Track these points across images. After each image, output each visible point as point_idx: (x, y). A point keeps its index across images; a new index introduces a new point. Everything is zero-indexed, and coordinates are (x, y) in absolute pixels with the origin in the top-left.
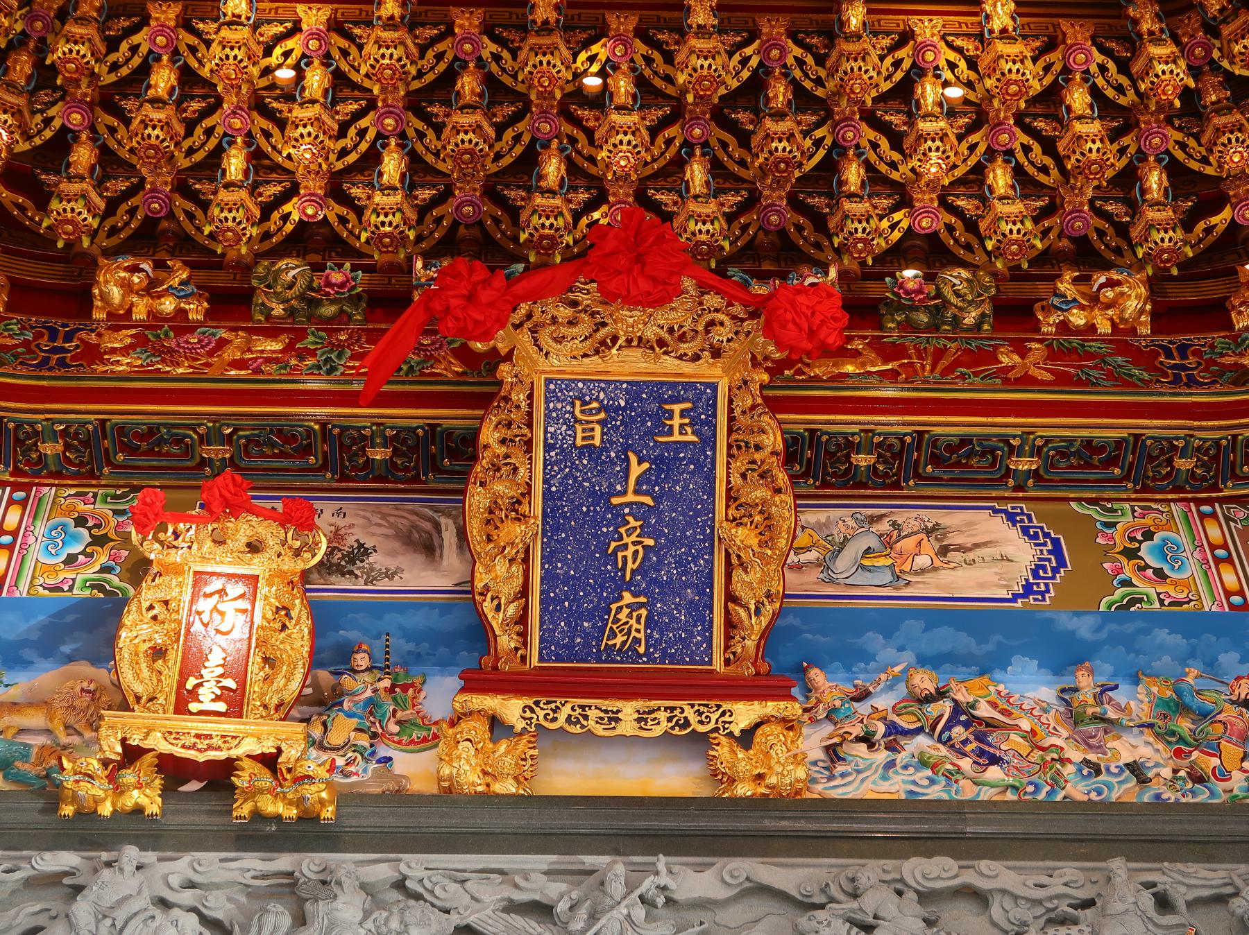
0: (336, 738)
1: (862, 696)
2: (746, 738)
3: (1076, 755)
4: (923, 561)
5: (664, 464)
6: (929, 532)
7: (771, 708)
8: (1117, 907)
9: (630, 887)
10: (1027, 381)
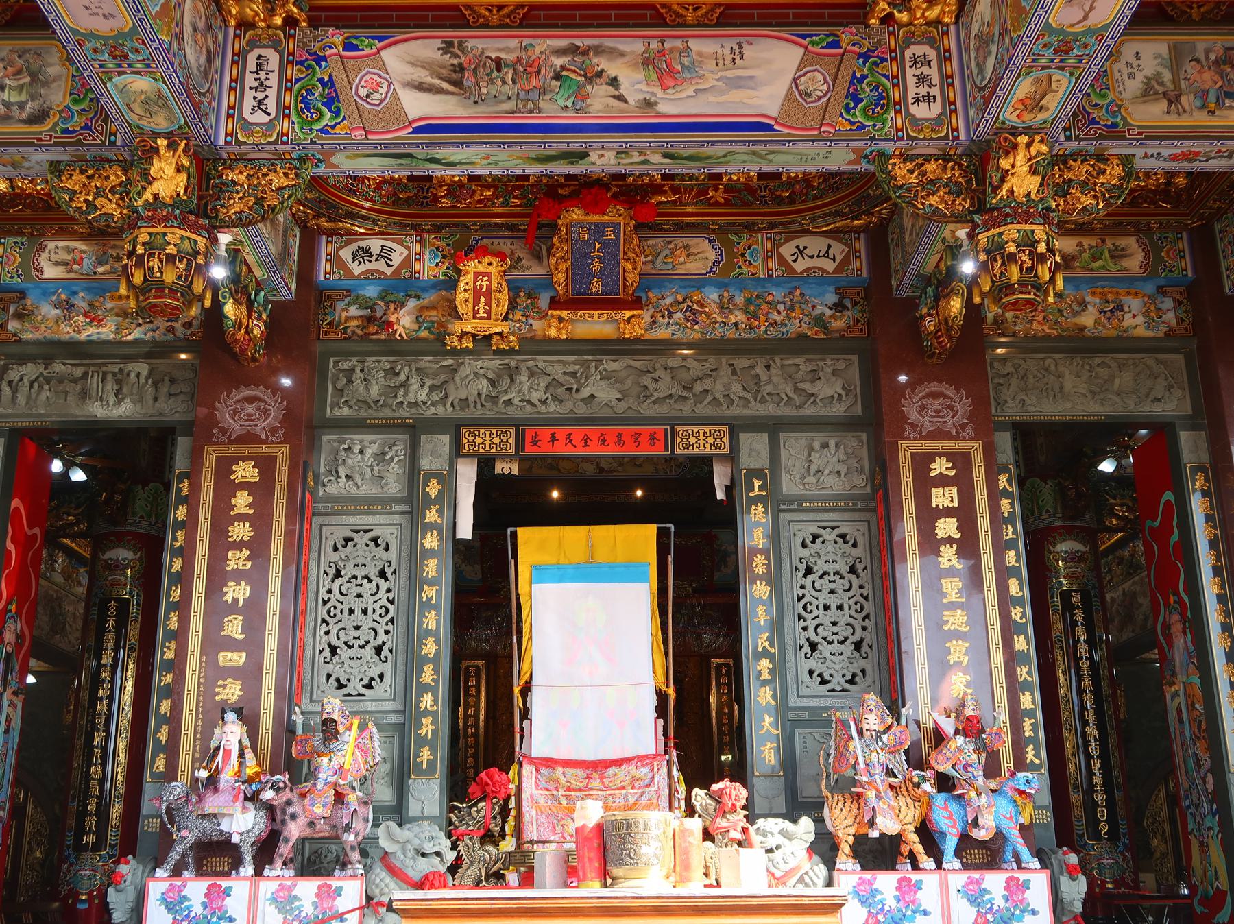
0: (516, 318)
1: (663, 298)
2: (628, 320)
3: (719, 320)
4: (682, 259)
5: (606, 244)
6: (685, 247)
7: (635, 312)
8: (721, 373)
9: (597, 368)
10: (717, 204)
